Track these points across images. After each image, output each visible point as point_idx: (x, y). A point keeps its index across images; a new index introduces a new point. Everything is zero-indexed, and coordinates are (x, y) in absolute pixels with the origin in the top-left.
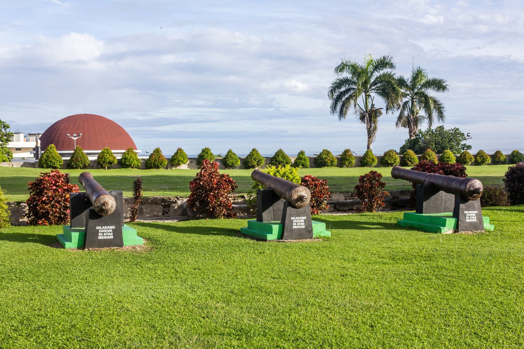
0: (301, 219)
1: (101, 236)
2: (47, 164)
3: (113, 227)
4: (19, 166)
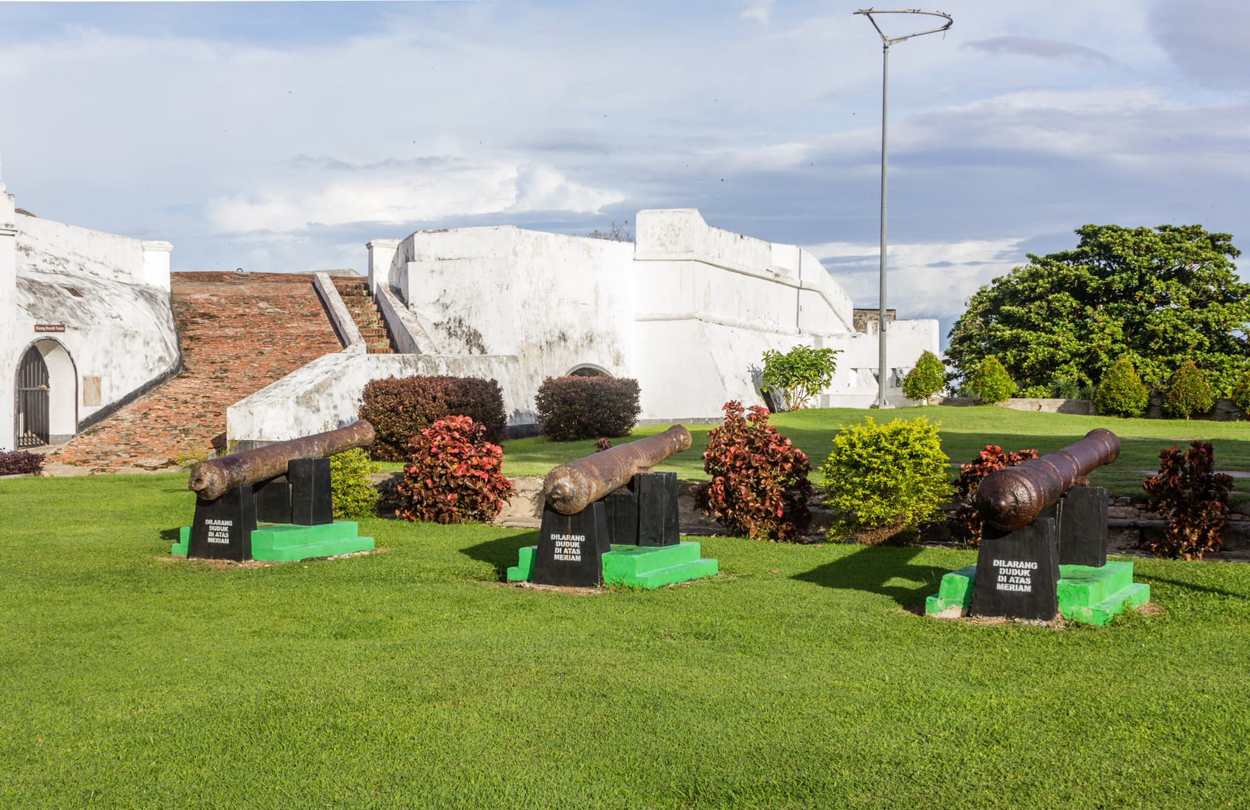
0: (573, 541)
1: (1003, 582)
2: (1105, 405)
4: (1054, 410)
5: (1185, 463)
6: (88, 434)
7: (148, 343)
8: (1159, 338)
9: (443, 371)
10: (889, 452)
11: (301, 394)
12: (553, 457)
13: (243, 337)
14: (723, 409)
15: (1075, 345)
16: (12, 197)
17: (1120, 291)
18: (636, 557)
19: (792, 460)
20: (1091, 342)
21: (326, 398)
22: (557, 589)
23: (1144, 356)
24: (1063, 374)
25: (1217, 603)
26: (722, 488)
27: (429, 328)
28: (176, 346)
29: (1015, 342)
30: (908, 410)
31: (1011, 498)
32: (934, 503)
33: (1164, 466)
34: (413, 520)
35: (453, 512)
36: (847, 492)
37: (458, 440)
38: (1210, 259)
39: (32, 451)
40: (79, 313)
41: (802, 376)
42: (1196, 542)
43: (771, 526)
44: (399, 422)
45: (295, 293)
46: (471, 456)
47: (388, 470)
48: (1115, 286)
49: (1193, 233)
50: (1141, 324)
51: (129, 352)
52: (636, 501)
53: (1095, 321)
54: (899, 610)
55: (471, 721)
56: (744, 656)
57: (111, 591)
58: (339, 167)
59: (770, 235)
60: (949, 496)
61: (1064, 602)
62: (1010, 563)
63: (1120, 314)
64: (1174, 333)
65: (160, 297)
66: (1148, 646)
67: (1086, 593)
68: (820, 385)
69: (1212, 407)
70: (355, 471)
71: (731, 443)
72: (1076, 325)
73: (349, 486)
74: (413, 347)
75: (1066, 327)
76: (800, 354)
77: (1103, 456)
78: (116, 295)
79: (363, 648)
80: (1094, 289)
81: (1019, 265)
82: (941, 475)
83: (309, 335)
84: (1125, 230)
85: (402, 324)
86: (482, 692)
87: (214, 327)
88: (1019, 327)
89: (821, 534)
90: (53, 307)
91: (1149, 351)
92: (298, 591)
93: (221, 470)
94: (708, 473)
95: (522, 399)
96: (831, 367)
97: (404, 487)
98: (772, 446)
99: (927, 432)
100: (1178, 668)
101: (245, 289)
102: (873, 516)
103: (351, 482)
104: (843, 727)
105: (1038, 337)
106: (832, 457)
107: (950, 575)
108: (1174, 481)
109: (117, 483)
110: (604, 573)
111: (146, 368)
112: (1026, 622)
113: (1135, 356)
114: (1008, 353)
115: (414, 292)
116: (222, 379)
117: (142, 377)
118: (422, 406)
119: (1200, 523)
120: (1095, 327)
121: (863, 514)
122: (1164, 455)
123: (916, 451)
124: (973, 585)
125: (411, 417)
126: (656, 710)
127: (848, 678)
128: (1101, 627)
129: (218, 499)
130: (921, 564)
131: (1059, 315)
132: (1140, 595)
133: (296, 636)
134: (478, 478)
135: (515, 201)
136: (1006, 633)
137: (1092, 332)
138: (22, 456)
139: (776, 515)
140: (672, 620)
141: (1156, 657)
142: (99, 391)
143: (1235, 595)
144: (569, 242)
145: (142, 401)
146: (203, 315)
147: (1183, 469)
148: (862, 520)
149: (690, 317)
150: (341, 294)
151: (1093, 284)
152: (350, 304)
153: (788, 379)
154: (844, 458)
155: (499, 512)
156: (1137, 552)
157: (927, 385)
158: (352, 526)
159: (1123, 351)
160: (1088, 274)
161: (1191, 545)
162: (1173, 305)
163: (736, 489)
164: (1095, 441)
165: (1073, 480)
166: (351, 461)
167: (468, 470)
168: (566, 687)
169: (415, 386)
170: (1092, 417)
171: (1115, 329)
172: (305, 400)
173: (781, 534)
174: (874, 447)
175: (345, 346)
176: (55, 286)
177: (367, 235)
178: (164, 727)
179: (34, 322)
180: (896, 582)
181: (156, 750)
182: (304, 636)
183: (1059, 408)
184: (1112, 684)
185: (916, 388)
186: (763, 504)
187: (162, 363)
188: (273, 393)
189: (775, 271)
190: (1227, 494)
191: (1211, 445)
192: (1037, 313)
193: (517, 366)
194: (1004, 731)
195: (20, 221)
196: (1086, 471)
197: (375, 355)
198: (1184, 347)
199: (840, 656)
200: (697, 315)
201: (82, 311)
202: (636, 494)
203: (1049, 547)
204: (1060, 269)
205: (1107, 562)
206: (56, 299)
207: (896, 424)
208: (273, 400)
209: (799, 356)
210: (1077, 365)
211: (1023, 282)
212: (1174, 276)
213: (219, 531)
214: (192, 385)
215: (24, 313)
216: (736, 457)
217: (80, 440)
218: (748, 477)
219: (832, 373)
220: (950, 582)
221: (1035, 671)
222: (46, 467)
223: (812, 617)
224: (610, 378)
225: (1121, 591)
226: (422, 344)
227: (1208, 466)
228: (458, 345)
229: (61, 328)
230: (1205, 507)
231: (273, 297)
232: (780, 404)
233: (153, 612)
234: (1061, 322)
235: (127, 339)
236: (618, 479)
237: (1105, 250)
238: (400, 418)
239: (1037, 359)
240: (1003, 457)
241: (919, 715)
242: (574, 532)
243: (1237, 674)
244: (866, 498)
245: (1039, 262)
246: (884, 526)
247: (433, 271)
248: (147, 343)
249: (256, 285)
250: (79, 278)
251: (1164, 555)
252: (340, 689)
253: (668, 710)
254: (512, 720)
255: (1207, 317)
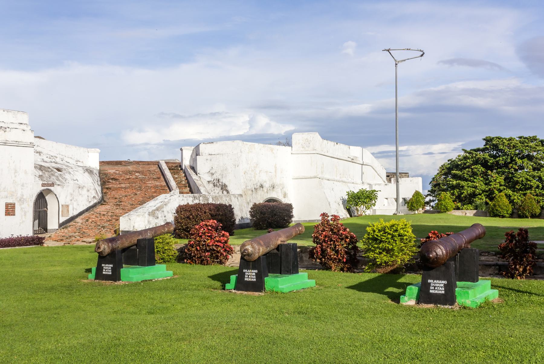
1: (433, 289)
2: (493, 213)
3: (445, 282)
4: (472, 215)
5: (516, 238)
6: (63, 228)
7: (89, 191)
8: (520, 184)
9: (210, 201)
10: (389, 234)
11: (151, 211)
12: (254, 237)
13: (129, 188)
14: (320, 216)
15: (484, 187)
16: (33, 132)
17: (502, 164)
18: (279, 279)
19: (349, 238)
20: (491, 186)
21: (161, 213)
22: (246, 293)
23: (514, 191)
24: (479, 199)
25: (527, 298)
26: (320, 250)
27: (205, 183)
28: (101, 192)
29: (458, 186)
30: (409, 216)
31: (435, 254)
32: (410, 255)
33: (507, 239)
34: (191, 264)
35: (208, 260)
36: (373, 251)
37: (211, 230)
38: (541, 150)
39: (40, 236)
40: (60, 178)
41: (363, 202)
42: (522, 271)
43: (341, 265)
44: (190, 223)
45: (151, 169)
46: (216, 237)
47: (183, 242)
48: (500, 162)
49: (533, 139)
50: (512, 178)
51: (81, 194)
52: (280, 255)
53: (492, 177)
54: (390, 301)
55: (195, 349)
56: (317, 321)
57: (60, 294)
58: (177, 117)
59: (350, 143)
60: (416, 252)
61: (459, 298)
62: (435, 281)
63: (503, 174)
64: (526, 182)
65: (95, 171)
66: (493, 317)
67: (468, 294)
68: (371, 205)
69: (540, 213)
70: (168, 243)
71: (324, 230)
72: (484, 179)
73: (165, 250)
74: (199, 191)
75: (480, 180)
76: (362, 192)
77: (478, 235)
78: (76, 171)
79: (156, 318)
80: (491, 163)
81: (461, 154)
82: (413, 243)
83: (156, 187)
84: (504, 138)
85: (194, 181)
86: (201, 337)
87: (117, 184)
88: (460, 180)
89: (363, 269)
90: (49, 176)
91: (516, 190)
92: (137, 294)
93: (108, 244)
94: (314, 243)
95: (244, 212)
96: (376, 198)
97: (188, 250)
98: (341, 232)
99: (406, 225)
100: (503, 326)
101: (130, 168)
102: (383, 261)
103: (166, 248)
104: (353, 352)
105: (468, 184)
106: (366, 236)
107: (410, 286)
108: (511, 245)
109: (72, 249)
110: (265, 286)
111: (88, 201)
112: (443, 307)
113: (510, 192)
114: (455, 191)
115: (200, 168)
116: (119, 205)
117: (86, 205)
118: (200, 216)
119: (523, 263)
120: (492, 179)
121: (379, 260)
122: (507, 234)
123: (401, 233)
124: (420, 291)
125: (195, 220)
126: (274, 345)
127: (360, 331)
128: (475, 309)
129: (107, 255)
130: (402, 282)
131: (477, 174)
132: (493, 295)
133: (132, 313)
134: (219, 246)
135: (248, 130)
136: (433, 311)
137: (491, 182)
138: (35, 238)
139: (343, 261)
140: (291, 306)
141: (495, 321)
142: (68, 211)
143: (535, 294)
144: (264, 147)
145: (86, 214)
146: (112, 179)
147: (516, 240)
148: (378, 263)
149: (315, 177)
150: (170, 169)
151: (491, 161)
152: (173, 174)
153: (357, 203)
154: (371, 236)
155: (228, 260)
156: (498, 276)
157: (417, 205)
158: (164, 266)
159: (504, 189)
160: (489, 157)
161: (520, 273)
162: (525, 170)
163: (326, 250)
164: (474, 229)
165: (463, 245)
166: (166, 239)
167: (214, 243)
168: (237, 335)
169: (197, 207)
170: (488, 218)
171: (501, 180)
172: (152, 214)
173: (345, 269)
174: (383, 232)
175: (170, 191)
176: (51, 167)
177: (180, 146)
178: (68, 352)
179: (41, 182)
180: (390, 289)
181: (63, 361)
182: (135, 313)
183: (474, 214)
184: (473, 333)
185: (413, 206)
186: (337, 256)
187: (94, 199)
188: (139, 211)
189: (352, 158)
190: (535, 251)
191: (527, 230)
192: (467, 174)
193: (242, 199)
194: (421, 354)
195: (37, 141)
196: (470, 242)
197: (182, 195)
198: (531, 187)
199: (359, 321)
200: (318, 177)
201: (62, 178)
202: (280, 252)
203: (452, 274)
204: (476, 155)
205: (479, 280)
206: (51, 173)
207: (393, 222)
208: (139, 213)
209: (362, 193)
210: (485, 196)
211: (461, 161)
212: (525, 157)
213: (107, 269)
214: (107, 208)
215: (37, 179)
216: (325, 236)
217: (60, 231)
218: (331, 245)
219: (376, 200)
220: (410, 289)
221: (441, 328)
222: (46, 242)
223: (351, 304)
224: (281, 203)
225: (485, 293)
226: (202, 190)
227: (526, 238)
228: (218, 190)
229: (53, 185)
230: (525, 256)
231: (141, 171)
232: (354, 214)
233: (75, 303)
234: (477, 178)
235: (80, 189)
236: (272, 246)
237: (496, 147)
238: (191, 221)
239: (467, 193)
240: (438, 235)
241: (386, 347)
242: (253, 269)
243: (528, 329)
244: (380, 253)
245: (468, 152)
246: (388, 265)
247: (207, 160)
248: (88, 191)
249: (135, 166)
250: (61, 164)
251: (508, 277)
252: (143, 336)
253: (279, 345)
254: (212, 349)
255: (540, 175)
